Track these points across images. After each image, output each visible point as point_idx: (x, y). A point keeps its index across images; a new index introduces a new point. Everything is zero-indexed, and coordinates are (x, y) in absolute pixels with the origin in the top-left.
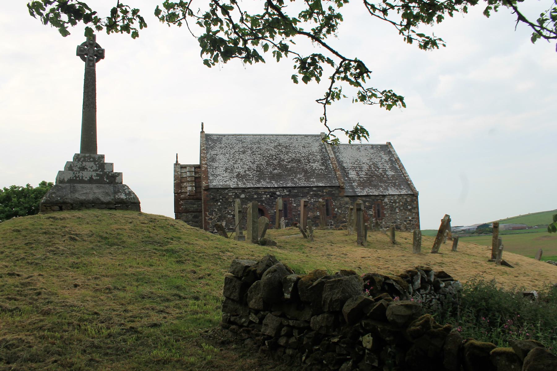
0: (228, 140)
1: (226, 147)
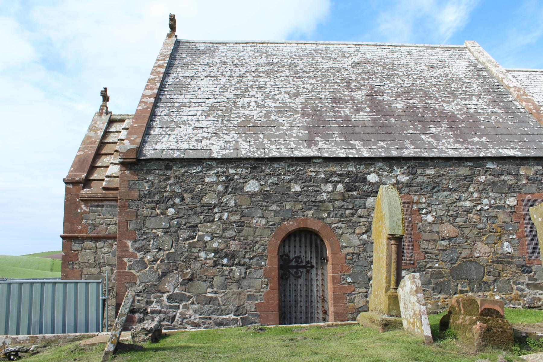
1: (225, 63)
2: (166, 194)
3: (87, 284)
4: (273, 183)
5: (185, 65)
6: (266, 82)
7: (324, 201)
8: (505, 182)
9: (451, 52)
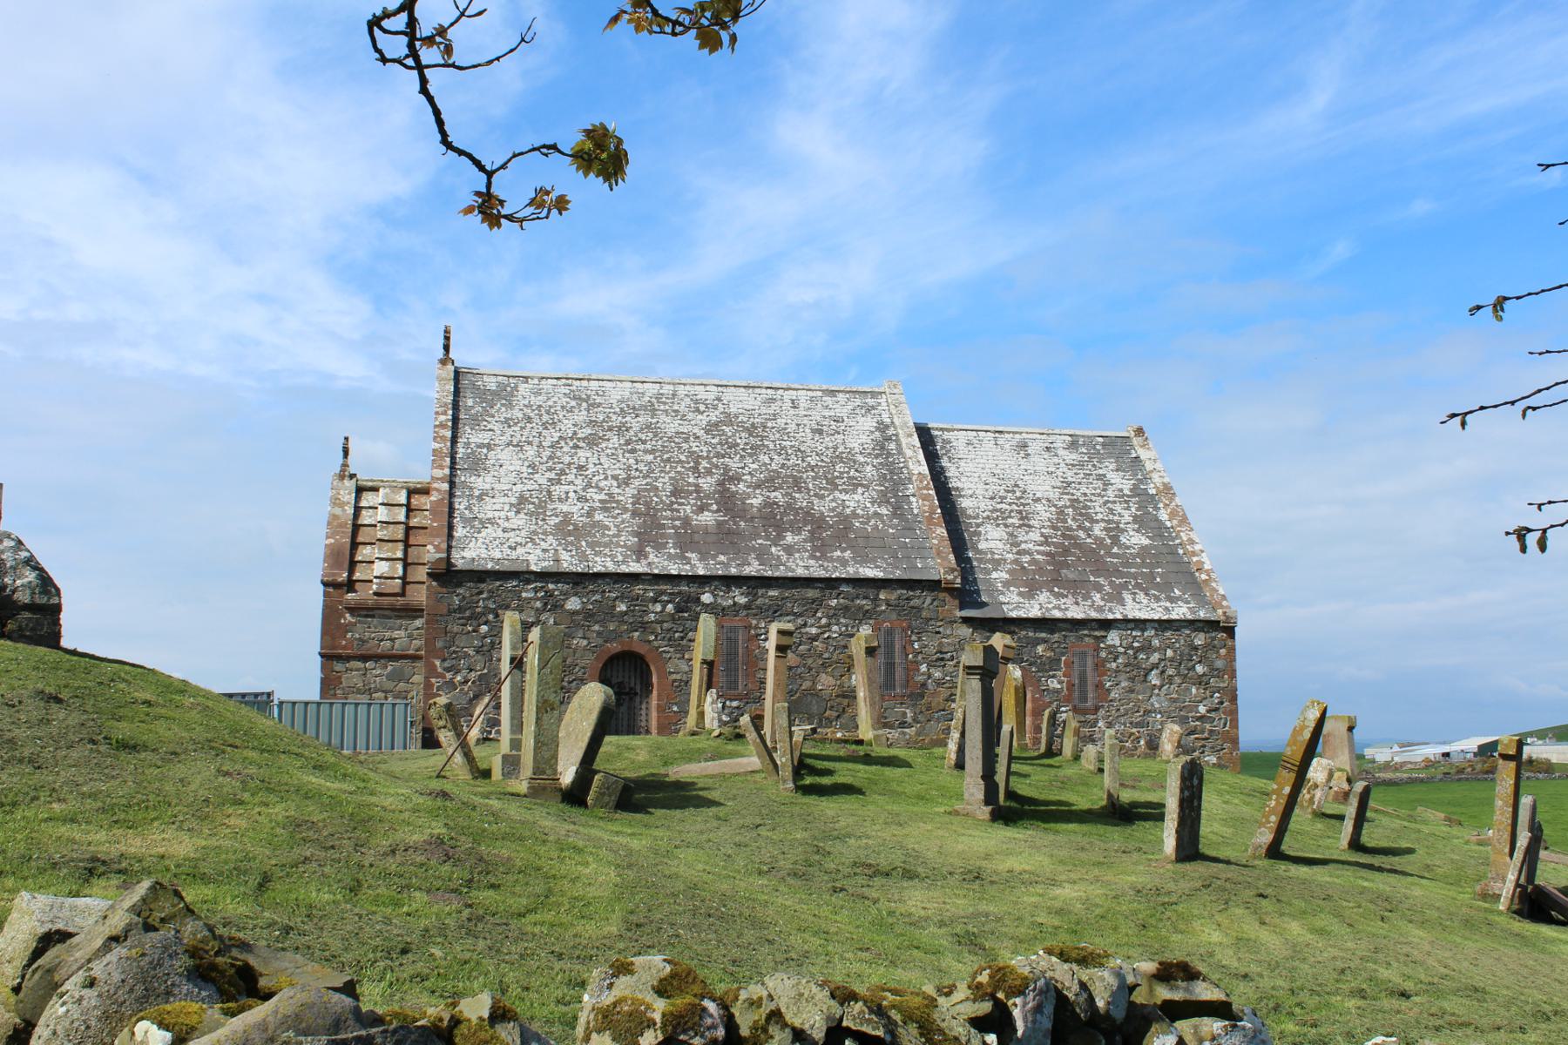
0: (538, 393)
1: (529, 420)
2: (478, 610)
3: (394, 705)
4: (596, 601)
5: (476, 421)
7: (652, 622)
8: (860, 607)
9: (858, 402)
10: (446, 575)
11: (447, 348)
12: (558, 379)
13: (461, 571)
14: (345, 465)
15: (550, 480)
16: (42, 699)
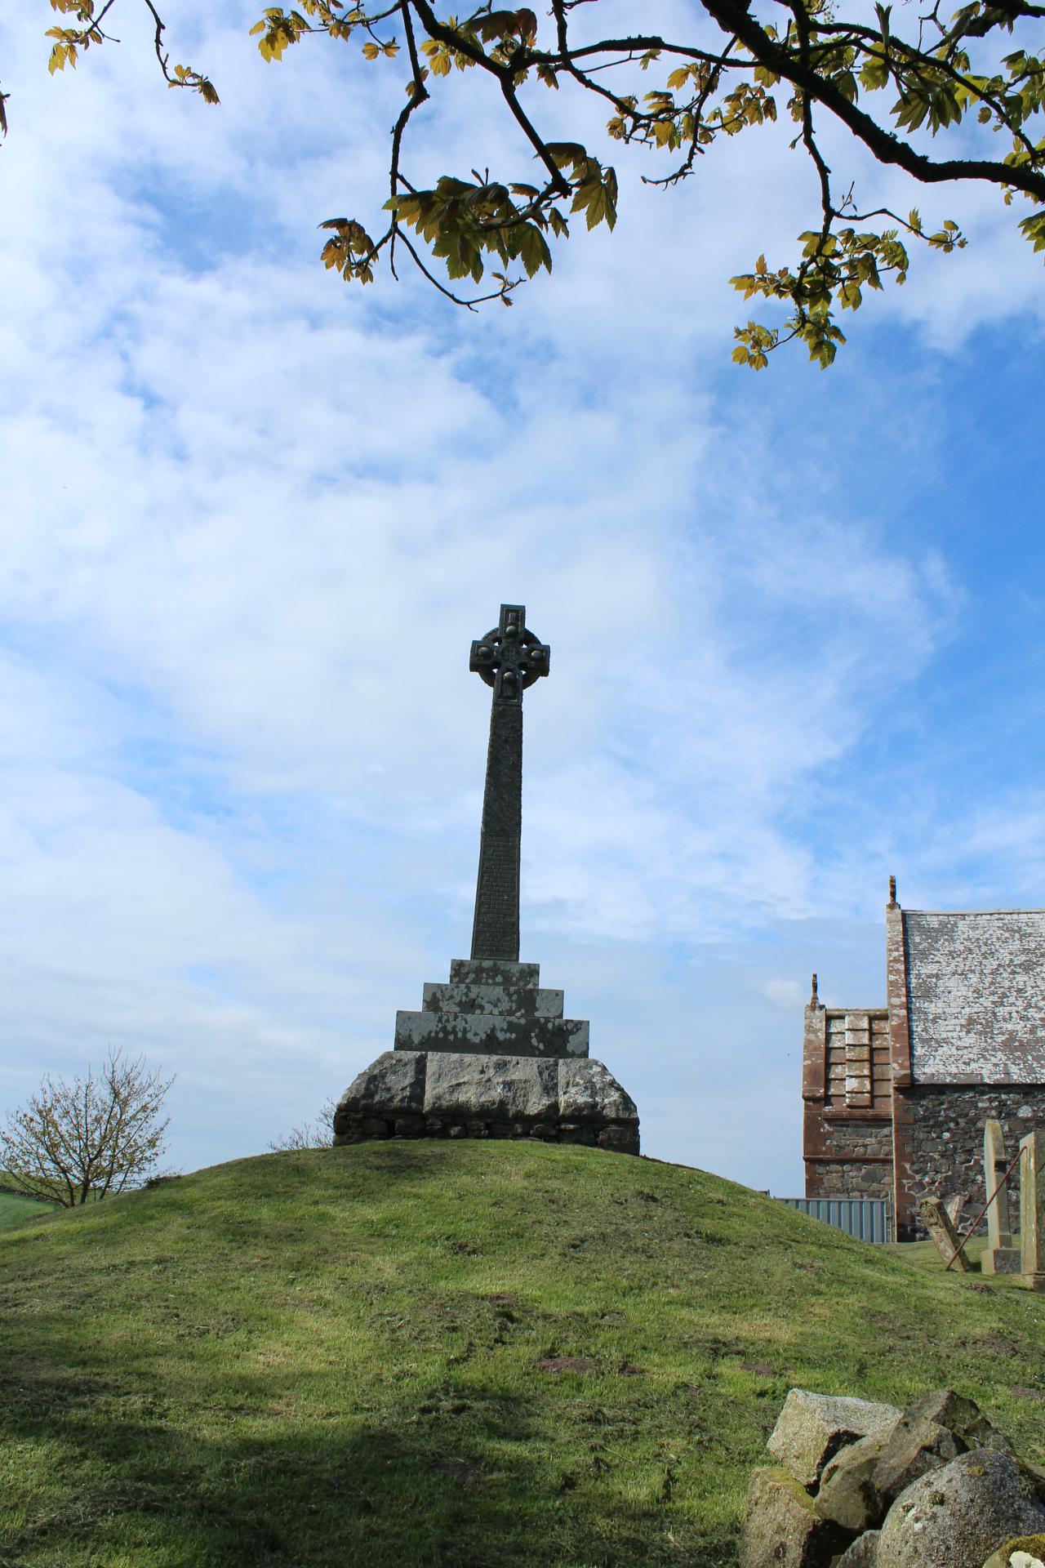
0: (975, 928)
1: (970, 951)
2: (941, 1119)
3: (872, 1203)
5: (924, 955)
6: (1025, 982)
10: (910, 1088)
11: (893, 894)
12: (991, 914)
13: (923, 1085)
14: (815, 998)
15: (993, 1003)
16: (642, 1198)
